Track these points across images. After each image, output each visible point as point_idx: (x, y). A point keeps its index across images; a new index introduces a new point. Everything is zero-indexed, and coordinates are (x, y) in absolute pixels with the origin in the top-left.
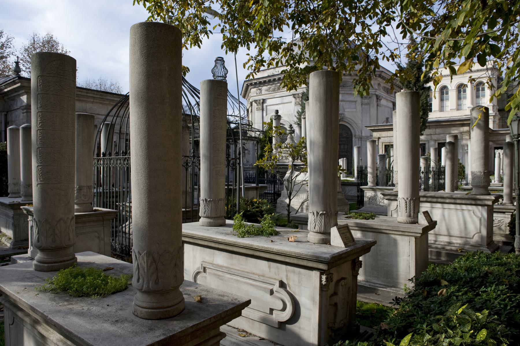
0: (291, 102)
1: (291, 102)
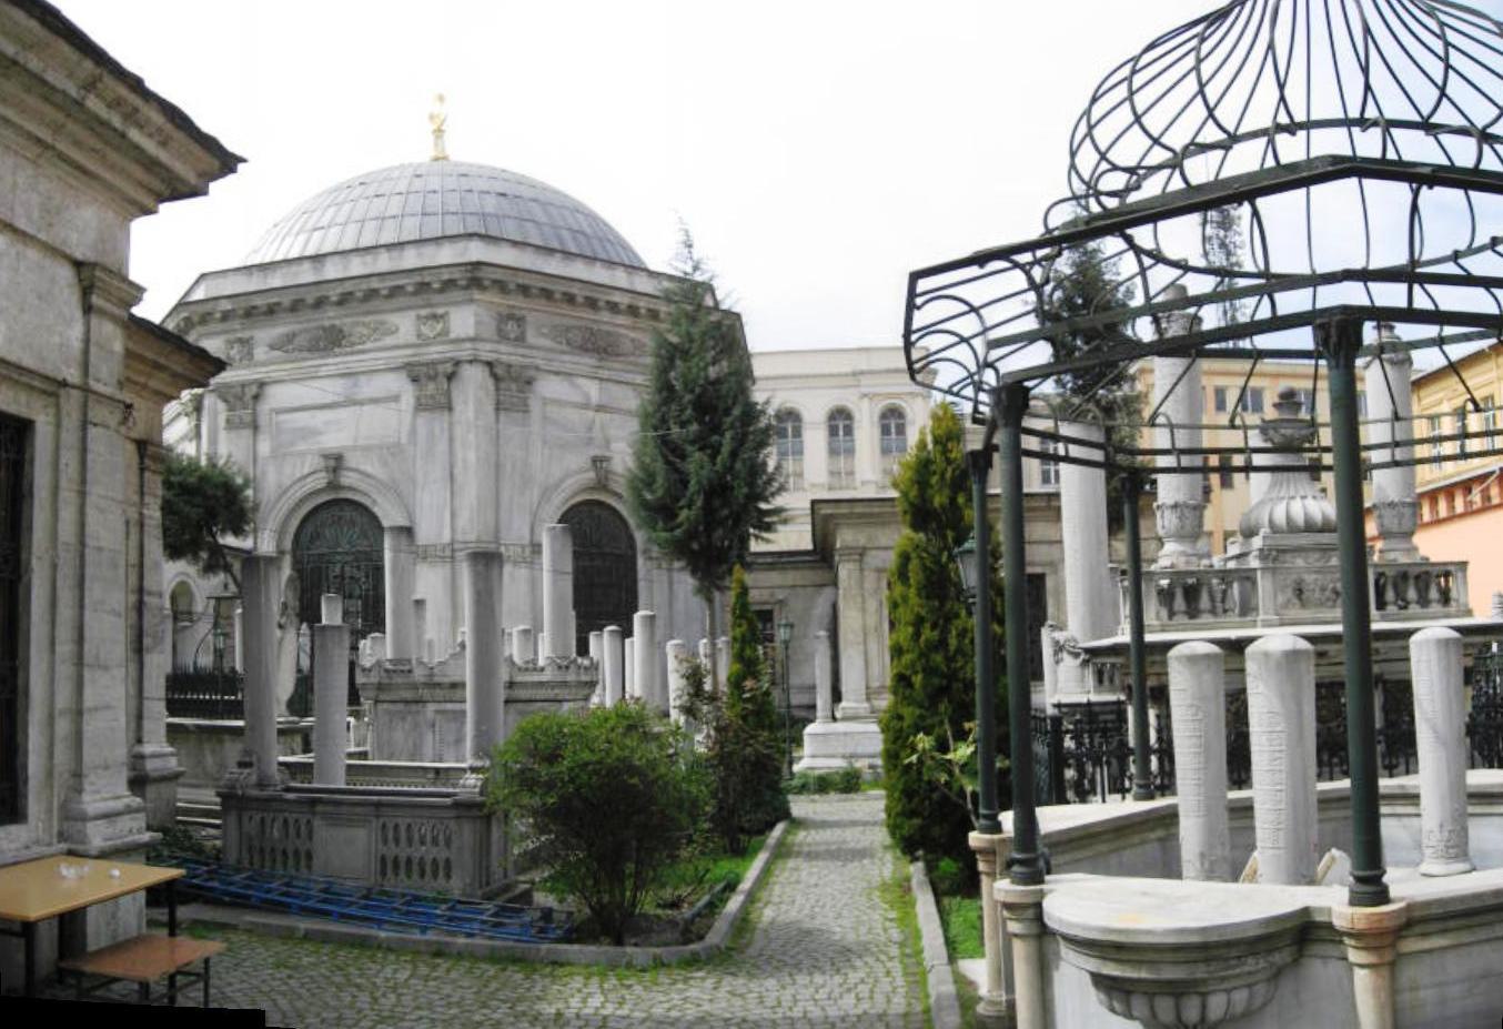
0: (396, 398)
1: (396, 398)
